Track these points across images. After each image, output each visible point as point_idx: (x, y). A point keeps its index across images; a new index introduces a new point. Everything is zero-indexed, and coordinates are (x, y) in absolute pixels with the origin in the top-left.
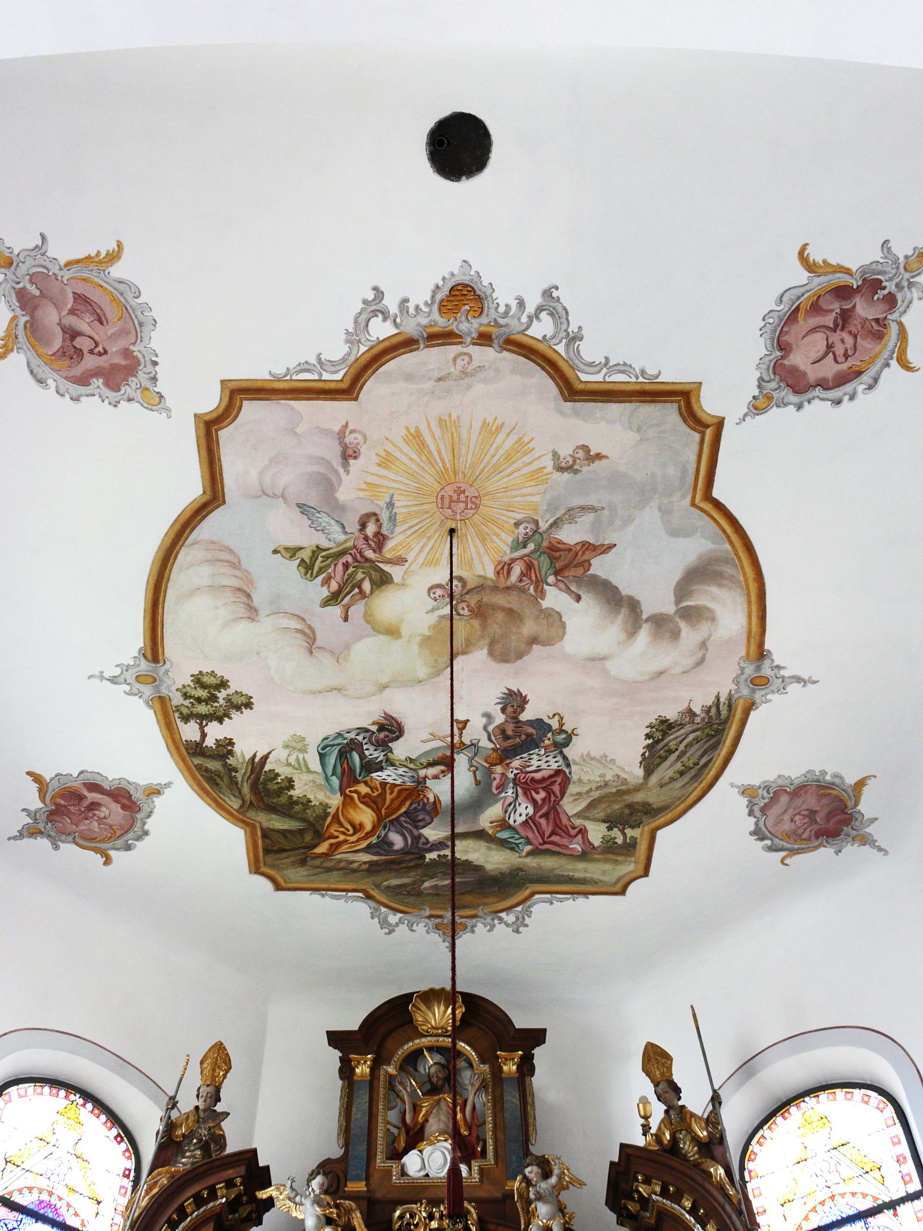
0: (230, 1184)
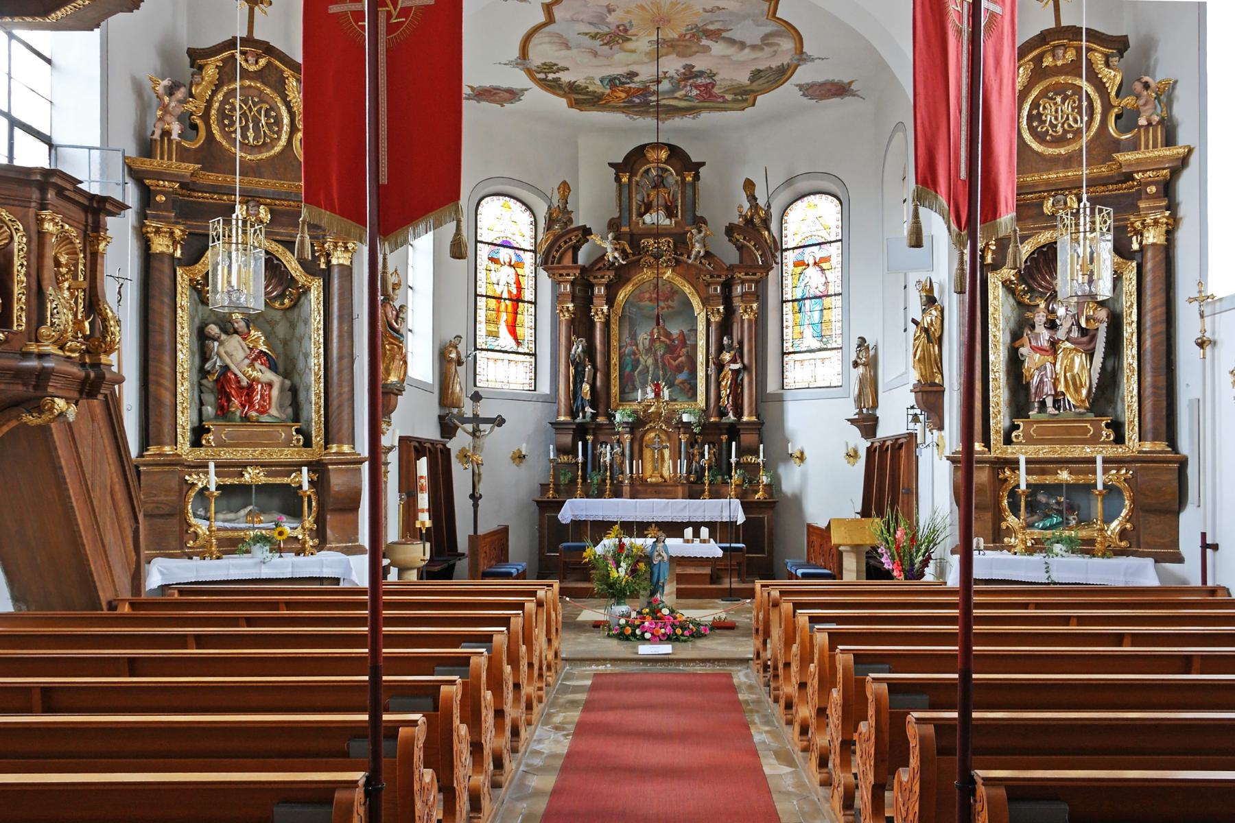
0: (576, 236)
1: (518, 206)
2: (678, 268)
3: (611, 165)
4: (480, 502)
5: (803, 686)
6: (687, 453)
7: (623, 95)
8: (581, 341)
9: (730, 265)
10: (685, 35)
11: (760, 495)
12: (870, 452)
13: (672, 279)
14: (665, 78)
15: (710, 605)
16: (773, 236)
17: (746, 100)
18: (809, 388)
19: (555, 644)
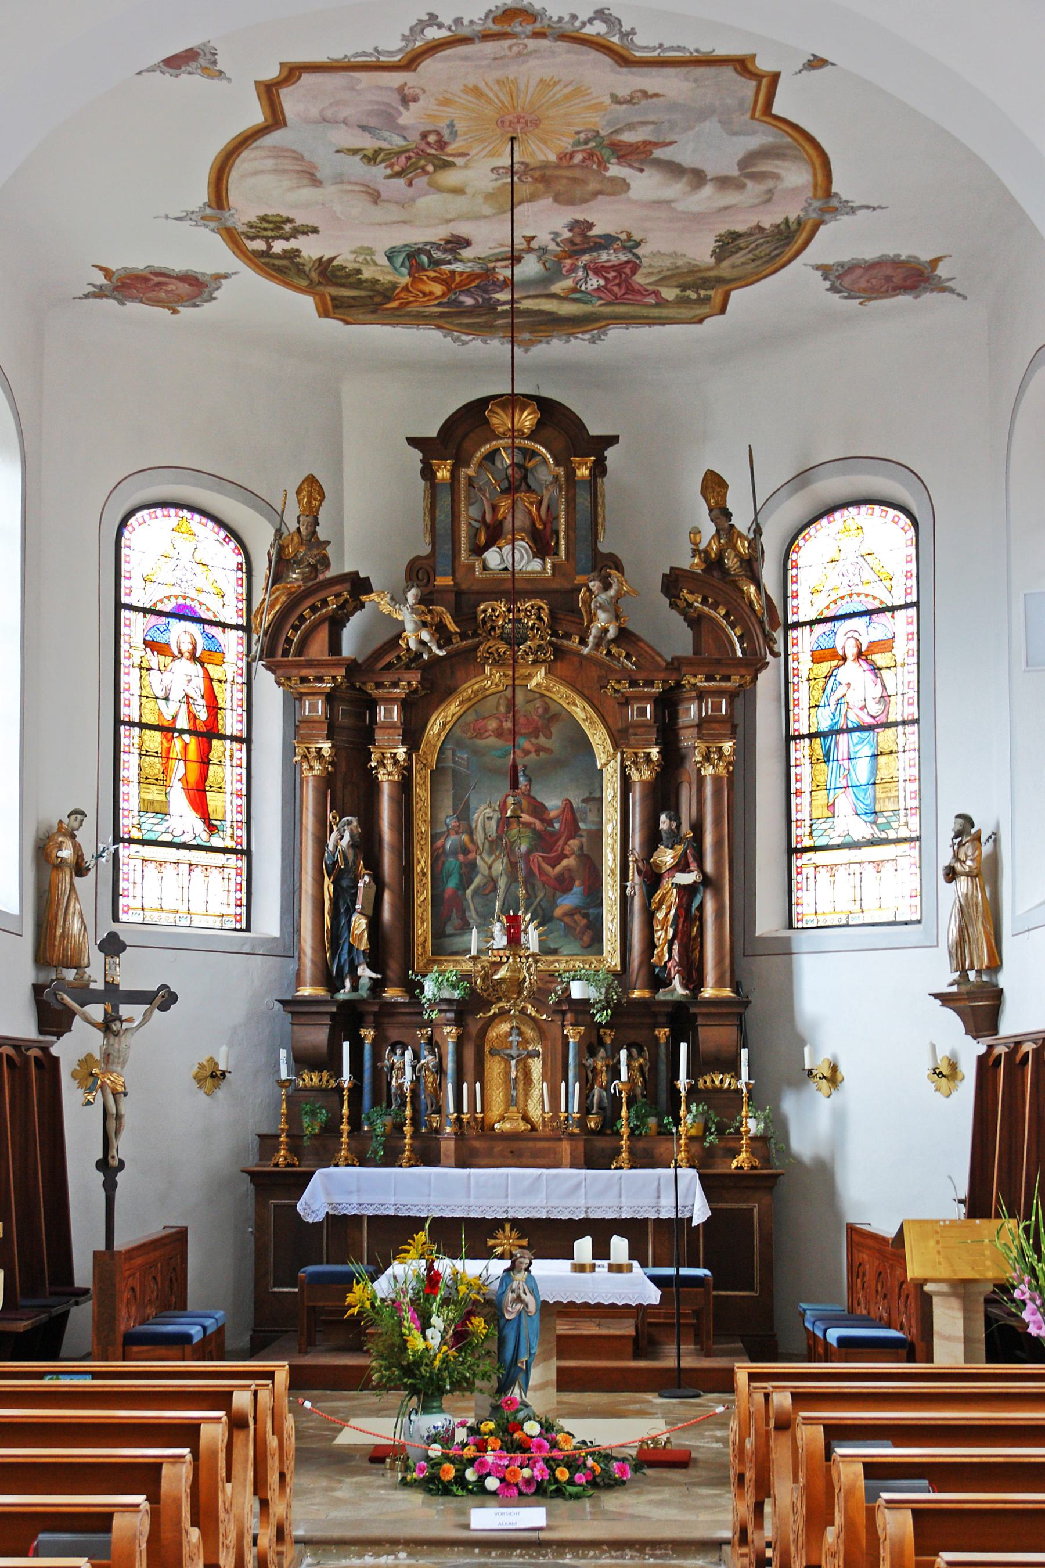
0: (338, 595)
1: (207, 532)
2: (559, 664)
3: (413, 442)
4: (120, 1177)
6: (581, 1066)
7: (438, 289)
8: (349, 823)
11: (742, 1159)
12: (986, 1065)
13: (548, 689)
14: (530, 250)
15: (632, 1407)
16: (767, 597)
17: (707, 299)
18: (847, 925)
19: (278, 1509)
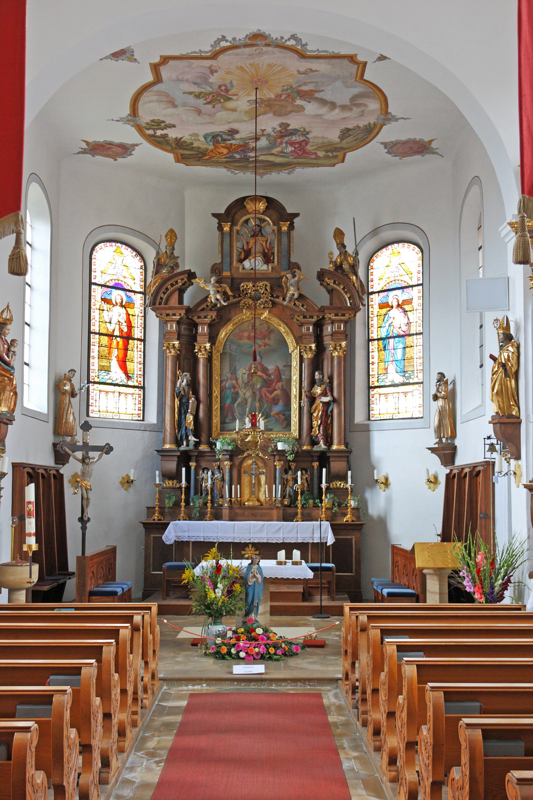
0: (182, 279)
1: (128, 252)
2: (274, 309)
3: (215, 215)
4: (88, 525)
5: (391, 715)
6: (282, 478)
7: (225, 151)
8: (186, 375)
9: (322, 307)
10: (281, 96)
11: (348, 518)
12: (449, 478)
13: (269, 319)
14: (263, 135)
16: (361, 281)
17: (336, 157)
18: (392, 419)
